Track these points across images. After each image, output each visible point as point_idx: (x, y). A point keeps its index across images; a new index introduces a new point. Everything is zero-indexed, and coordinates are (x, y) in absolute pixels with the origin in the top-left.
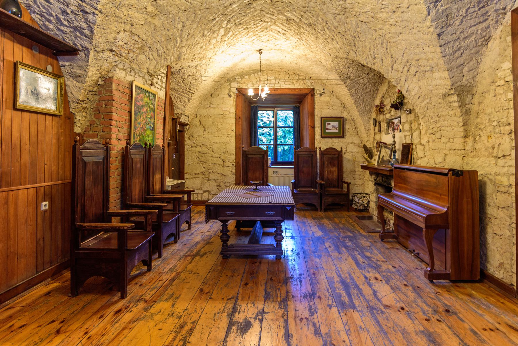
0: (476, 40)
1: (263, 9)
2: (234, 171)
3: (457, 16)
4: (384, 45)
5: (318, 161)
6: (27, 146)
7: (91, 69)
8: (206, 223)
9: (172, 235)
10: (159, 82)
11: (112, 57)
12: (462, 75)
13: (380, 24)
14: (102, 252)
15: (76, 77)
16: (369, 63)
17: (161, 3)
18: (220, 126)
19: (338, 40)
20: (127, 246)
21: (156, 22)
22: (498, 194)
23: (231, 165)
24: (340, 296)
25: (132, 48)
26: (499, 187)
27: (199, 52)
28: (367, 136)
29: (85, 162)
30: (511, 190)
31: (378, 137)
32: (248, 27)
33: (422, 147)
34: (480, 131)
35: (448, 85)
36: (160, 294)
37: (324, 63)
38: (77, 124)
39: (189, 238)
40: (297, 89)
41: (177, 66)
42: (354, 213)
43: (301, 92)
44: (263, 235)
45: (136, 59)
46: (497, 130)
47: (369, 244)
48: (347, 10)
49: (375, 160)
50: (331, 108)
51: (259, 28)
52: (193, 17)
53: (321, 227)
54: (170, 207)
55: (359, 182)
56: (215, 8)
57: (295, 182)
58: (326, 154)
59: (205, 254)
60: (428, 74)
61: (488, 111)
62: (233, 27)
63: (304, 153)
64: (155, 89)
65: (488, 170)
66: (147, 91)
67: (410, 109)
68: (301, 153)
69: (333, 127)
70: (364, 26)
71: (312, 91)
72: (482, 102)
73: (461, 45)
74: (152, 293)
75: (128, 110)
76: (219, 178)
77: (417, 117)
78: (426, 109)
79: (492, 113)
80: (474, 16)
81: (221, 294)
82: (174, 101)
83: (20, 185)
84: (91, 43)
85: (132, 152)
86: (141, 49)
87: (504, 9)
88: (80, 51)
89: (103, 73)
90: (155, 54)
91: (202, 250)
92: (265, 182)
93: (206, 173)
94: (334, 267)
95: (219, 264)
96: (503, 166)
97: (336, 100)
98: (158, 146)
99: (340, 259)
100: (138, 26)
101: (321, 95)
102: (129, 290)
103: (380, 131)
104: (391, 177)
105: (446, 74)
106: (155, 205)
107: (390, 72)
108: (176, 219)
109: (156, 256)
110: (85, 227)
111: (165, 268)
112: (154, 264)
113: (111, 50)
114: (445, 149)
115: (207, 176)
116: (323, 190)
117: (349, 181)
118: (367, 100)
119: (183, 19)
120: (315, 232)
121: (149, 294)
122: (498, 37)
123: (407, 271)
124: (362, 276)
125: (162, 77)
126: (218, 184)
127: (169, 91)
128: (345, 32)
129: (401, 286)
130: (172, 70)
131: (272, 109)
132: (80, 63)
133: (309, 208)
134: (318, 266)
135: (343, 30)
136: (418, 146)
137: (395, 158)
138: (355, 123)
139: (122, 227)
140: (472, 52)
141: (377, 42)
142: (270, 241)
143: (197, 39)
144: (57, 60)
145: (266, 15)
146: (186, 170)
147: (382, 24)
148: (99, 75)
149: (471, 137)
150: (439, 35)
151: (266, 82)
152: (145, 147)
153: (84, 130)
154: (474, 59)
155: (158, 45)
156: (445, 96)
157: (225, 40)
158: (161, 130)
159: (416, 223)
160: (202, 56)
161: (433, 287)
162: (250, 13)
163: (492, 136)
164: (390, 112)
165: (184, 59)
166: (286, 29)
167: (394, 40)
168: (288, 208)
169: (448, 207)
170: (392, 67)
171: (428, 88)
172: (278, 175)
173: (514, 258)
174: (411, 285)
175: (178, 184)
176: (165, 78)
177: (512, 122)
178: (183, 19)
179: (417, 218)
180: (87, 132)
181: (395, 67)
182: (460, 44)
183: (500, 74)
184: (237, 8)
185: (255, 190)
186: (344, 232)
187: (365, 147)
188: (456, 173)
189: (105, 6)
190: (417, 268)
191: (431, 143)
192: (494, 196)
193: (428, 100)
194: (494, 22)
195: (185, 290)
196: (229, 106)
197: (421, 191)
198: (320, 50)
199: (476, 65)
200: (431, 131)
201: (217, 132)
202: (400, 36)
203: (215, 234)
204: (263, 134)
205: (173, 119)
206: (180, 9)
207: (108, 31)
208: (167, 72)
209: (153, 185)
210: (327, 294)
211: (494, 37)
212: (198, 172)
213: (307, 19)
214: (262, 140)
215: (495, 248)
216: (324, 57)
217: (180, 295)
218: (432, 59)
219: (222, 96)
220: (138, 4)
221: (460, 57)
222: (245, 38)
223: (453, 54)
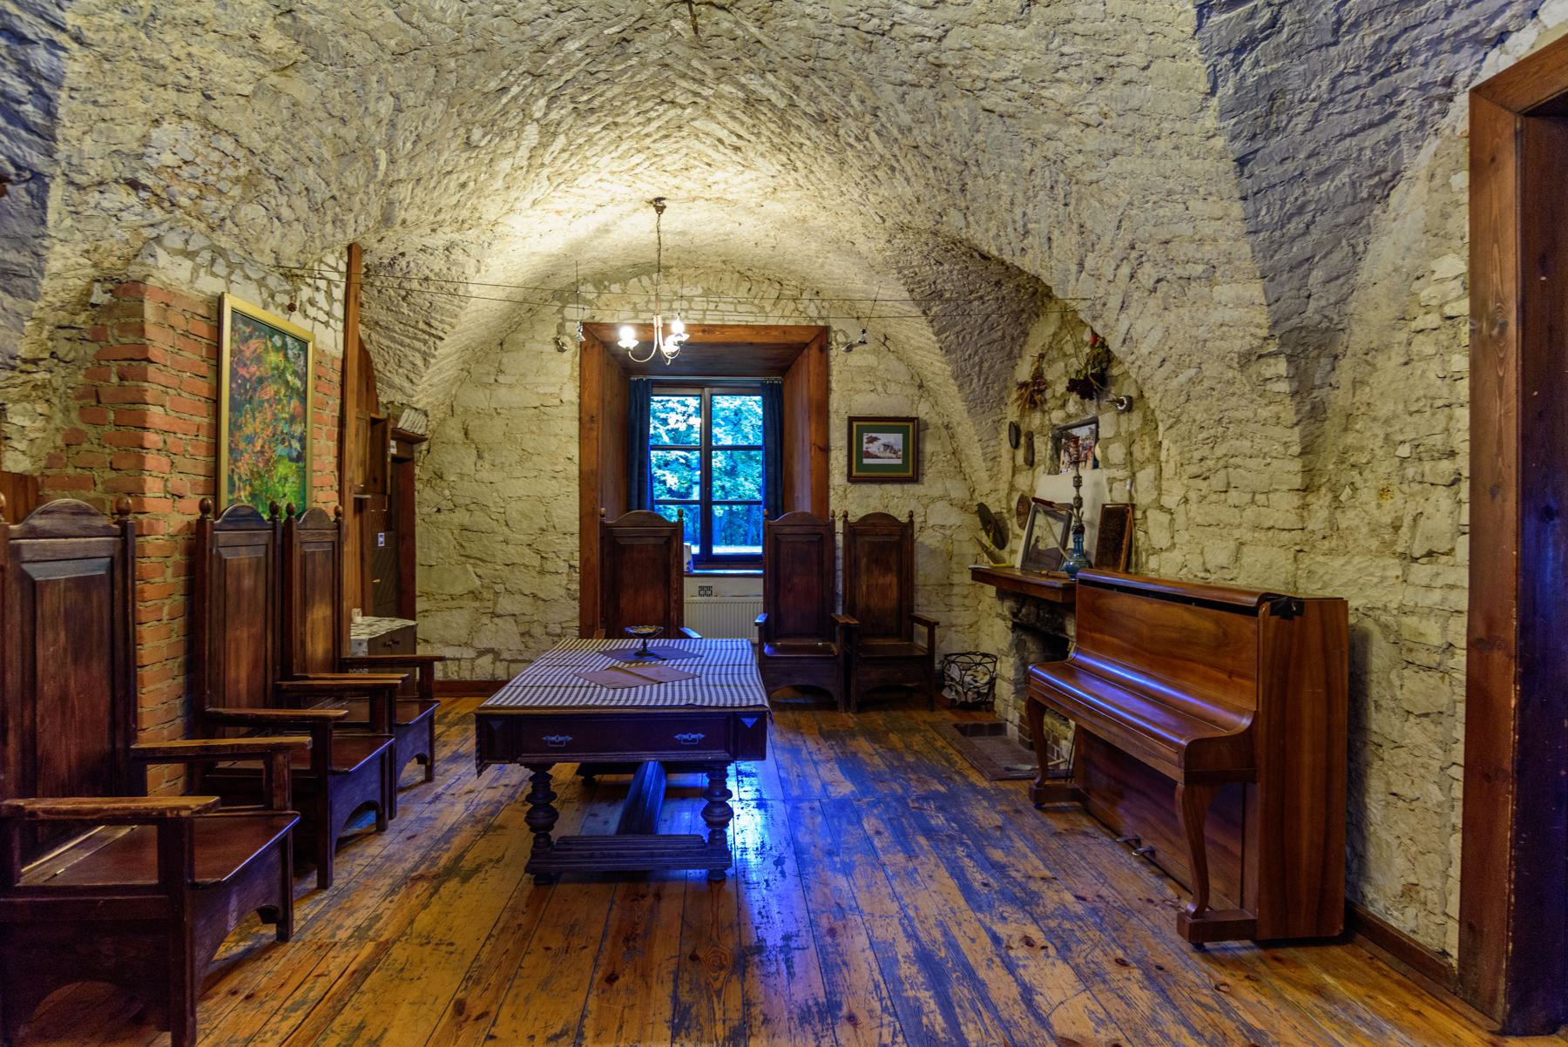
0: (1353, 183)
1: (669, 61)
2: (575, 587)
3: (1301, 102)
4: (1060, 191)
5: (840, 553)
7: (58, 248)
8: (479, 773)
9: (368, 806)
10: (321, 298)
11: (139, 209)
12: (1304, 293)
13: (1048, 121)
14: (102, 898)
16: (1007, 249)
17: (312, 23)
18: (530, 445)
19: (910, 173)
20: (192, 875)
21: (296, 87)
22: (1406, 673)
23: (566, 570)
24: (917, 1011)
25: (211, 179)
26: (1410, 650)
27: (454, 200)
28: (991, 477)
29: (34, 583)
30: (1451, 663)
31: (1022, 481)
32: (620, 120)
33: (1165, 518)
34: (1354, 473)
35: (1259, 326)
36: (317, 1029)
37: (863, 246)
38: (16, 444)
39: (426, 815)
40: (776, 327)
41: (383, 246)
42: (947, 714)
43: (789, 339)
44: (666, 797)
45: (232, 218)
46: (1410, 472)
47: (998, 820)
48: (945, 72)
49: (1013, 552)
50: (880, 389)
51: (655, 124)
52: (429, 80)
53: (851, 765)
54: (362, 711)
55: (962, 617)
56: (506, 52)
57: (767, 621)
58: (863, 534)
59: (478, 869)
60: (1195, 288)
61: (1385, 409)
62: (570, 120)
63: (795, 529)
64: (306, 325)
65: (1376, 596)
66: (275, 330)
67: (1130, 398)
68: (787, 530)
70: (998, 128)
71: (822, 336)
72: (1362, 382)
73: (1308, 197)
74: (286, 1027)
76: (528, 610)
77: (1150, 422)
78: (1183, 398)
80: (1354, 103)
81: (525, 1019)
82: (378, 362)
84: (49, 153)
85: (222, 536)
86: (249, 183)
87: (1448, 82)
88: (10, 181)
89: (106, 265)
90: (301, 204)
91: (469, 856)
92: (672, 626)
93: (486, 595)
94: (895, 907)
95: (522, 907)
96: (1428, 587)
97: (896, 363)
98: (322, 514)
99: (910, 874)
100: (229, 102)
101: (849, 348)
102: (205, 1020)
103: (1031, 463)
104: (1069, 608)
105: (1255, 291)
106: (304, 717)
107: (1072, 278)
108: (382, 755)
109: (312, 882)
110: (33, 813)
111: (339, 927)
112: (301, 913)
113: (134, 185)
114: (1240, 525)
115: (490, 604)
116: (851, 637)
117: (933, 617)
118: (991, 367)
119: (396, 82)
120: (831, 784)
121: (276, 1032)
122: (1423, 173)
123: (1123, 910)
124: (983, 934)
125: (329, 281)
126: (523, 628)
127: (355, 328)
128: (935, 145)
129: (1106, 965)
130: (367, 259)
131: (697, 392)
132: (15, 226)
133: (809, 700)
134: (844, 904)
135: (929, 139)
137: (1079, 549)
138: (952, 437)
139: (172, 809)
140: (1341, 219)
141: (1038, 181)
142: (686, 820)
143: (446, 155)
145: (678, 82)
146: (420, 584)
147: (1057, 122)
148: (91, 271)
149: (1323, 490)
150: (1242, 162)
151: (676, 305)
152: (271, 519)
153: (43, 464)
154: (1344, 242)
155: (311, 171)
156: (1248, 359)
157: (543, 165)
158: (330, 460)
159: (1151, 762)
160: (465, 213)
161: (1205, 966)
162: (624, 71)
164: (1063, 406)
165: (404, 222)
166: (742, 132)
167: (1093, 176)
168: (749, 722)
169: (1256, 716)
170: (1081, 265)
171: (1194, 332)
172: (712, 599)
173: (1455, 871)
174: (1138, 962)
175: (391, 634)
176: (343, 285)
177: (1464, 448)
178: (396, 82)
179: (1153, 748)
180: (55, 471)
181: (1090, 262)
182: (1304, 193)
183: (1427, 293)
184: (579, 55)
185: (643, 655)
186: (919, 780)
187: (982, 510)
188: (1285, 607)
189: (96, 20)
190: (1150, 901)
191: (1193, 506)
192: (1393, 676)
193: (1192, 372)
194: (1413, 124)
195: (405, 1009)
196: (557, 381)
197: (1162, 655)
198: (850, 205)
199: (1348, 263)
200: (1194, 469)
201: (520, 462)
202: (1112, 162)
203: (511, 797)
204: (667, 464)
205: (374, 422)
206: (382, 47)
207: (116, 112)
208: (349, 265)
209: (303, 643)
210: (877, 1006)
211: (1409, 174)
212: (459, 589)
213: (811, 98)
214: (664, 483)
215: (1390, 838)
216: (864, 226)
217: (386, 1030)
218: (1215, 240)
219: (537, 346)
220: (225, 19)
221: (1303, 234)
222: (607, 157)
223: (1283, 227)
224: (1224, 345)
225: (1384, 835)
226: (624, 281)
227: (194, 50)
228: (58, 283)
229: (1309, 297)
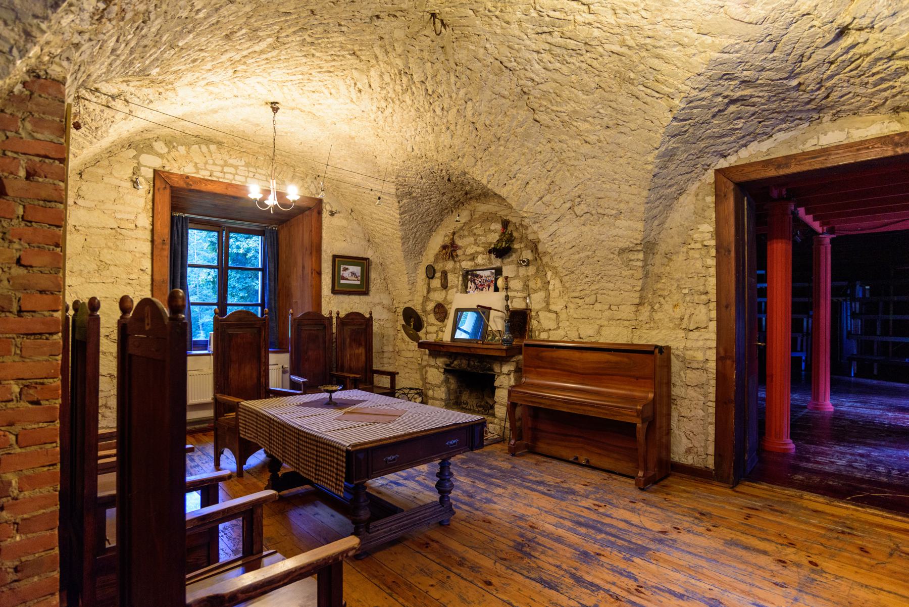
46: (688, 299)
50: (349, 240)
69: (350, 275)
78: (579, 263)
79: (683, 279)
105: (640, 226)
122: (693, 193)
136: (542, 314)
163: (680, 305)
167: (576, 163)
171: (598, 237)
192: (682, 373)
218: (628, 202)
224: (613, 244)
225: (677, 432)
226: (188, 146)
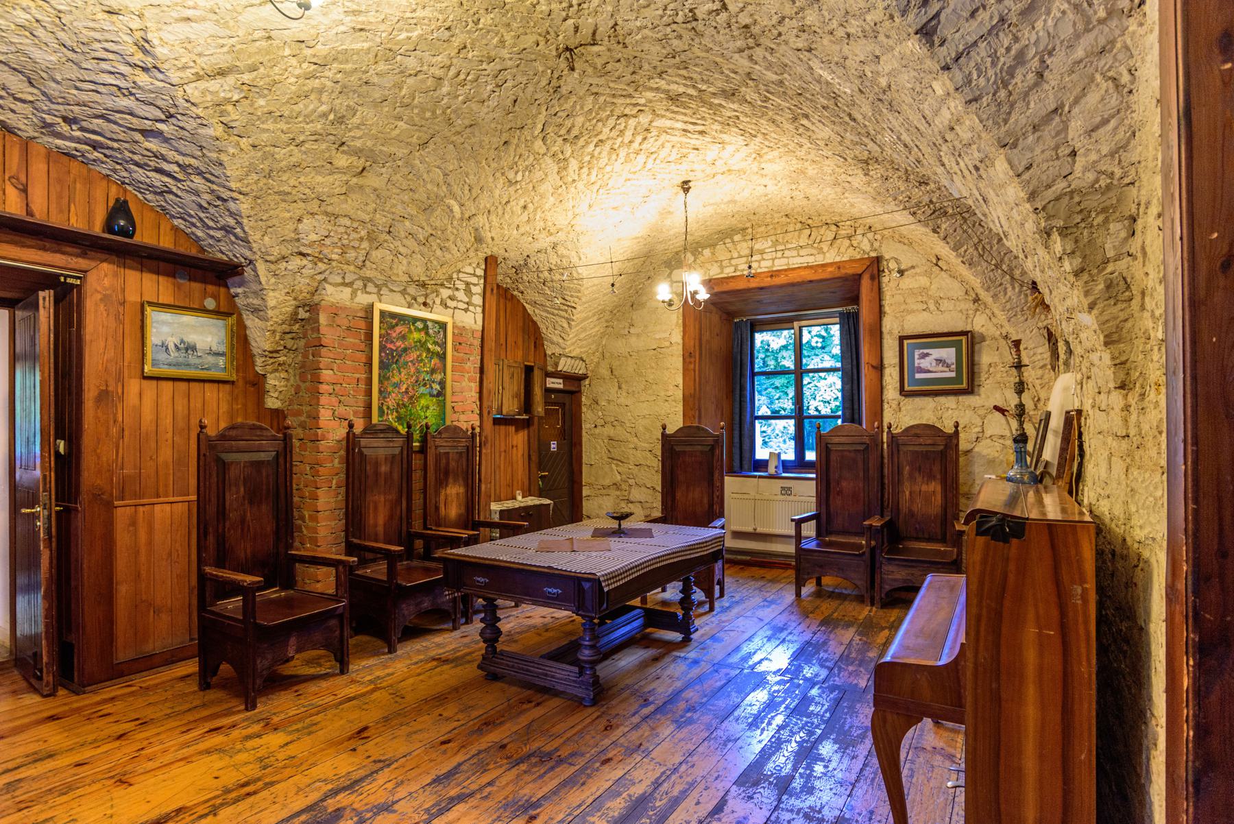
6: (170, 435)
7: (271, 294)
10: (461, 295)
11: (310, 265)
15: (256, 311)
18: (651, 377)
21: (373, 180)
29: (224, 463)
40: (831, 264)
50: (932, 307)
63: (843, 440)
68: (836, 440)
71: (875, 266)
73: (1024, 42)
75: (364, 360)
83: (158, 496)
86: (371, 237)
93: (624, 486)
97: (949, 280)
100: (335, 200)
140: (1080, 53)
144: (227, 287)
154: (1098, 78)
172: (791, 498)
182: (1016, 39)
199: (1114, 101)
201: (645, 390)
209: (437, 508)
212: (607, 482)
221: (1036, 85)
223: (1005, 86)
226: (713, 246)
227: (302, 180)
228: (277, 312)
229: (1074, 154)
